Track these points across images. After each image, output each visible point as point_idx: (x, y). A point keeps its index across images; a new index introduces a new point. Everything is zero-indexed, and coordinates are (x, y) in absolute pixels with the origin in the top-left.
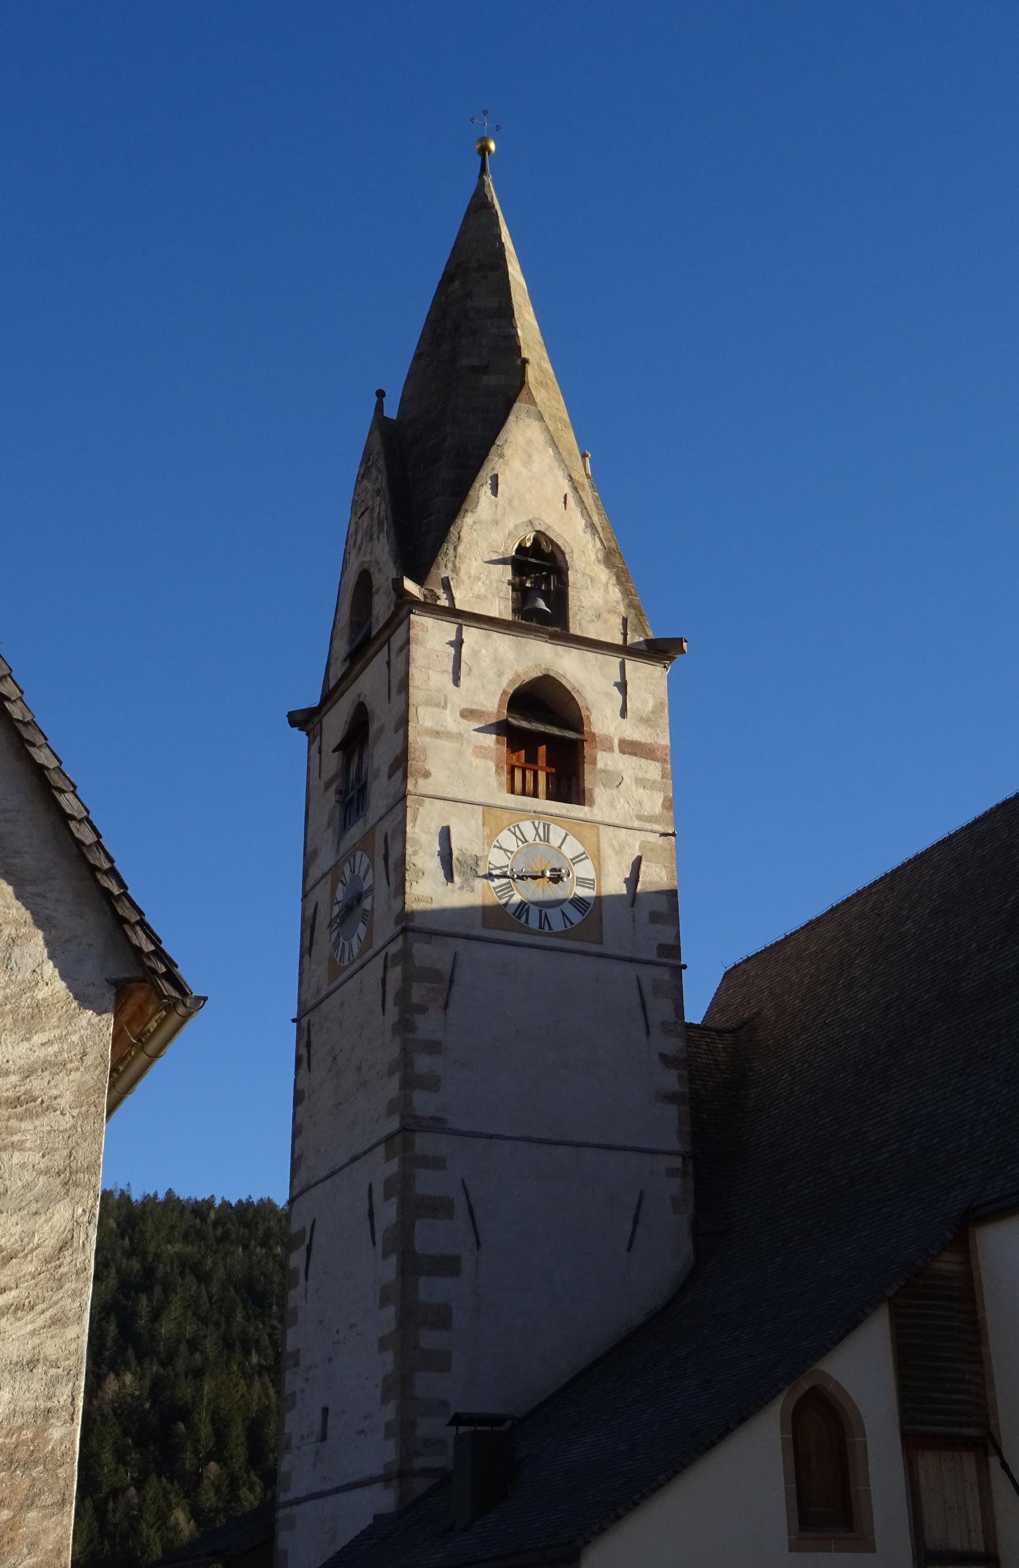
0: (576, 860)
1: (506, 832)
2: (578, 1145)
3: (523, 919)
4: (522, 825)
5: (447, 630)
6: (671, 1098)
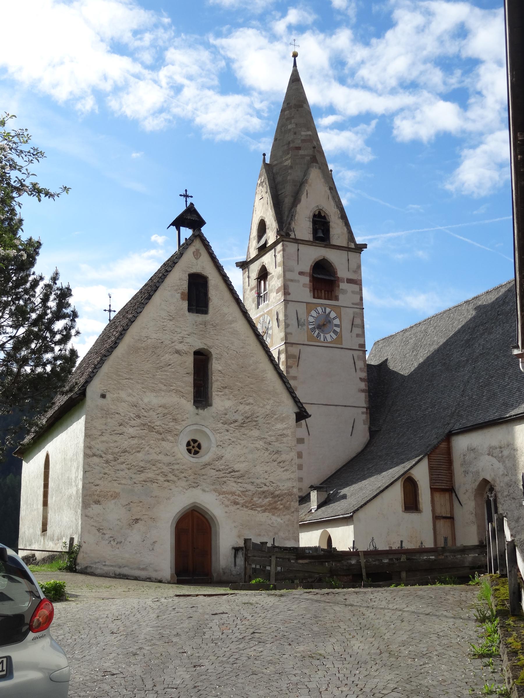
0: (334, 318)
1: (334, 338)
2: (336, 406)
3: (319, 338)
4: (318, 308)
5: (295, 246)
6: (363, 391)
